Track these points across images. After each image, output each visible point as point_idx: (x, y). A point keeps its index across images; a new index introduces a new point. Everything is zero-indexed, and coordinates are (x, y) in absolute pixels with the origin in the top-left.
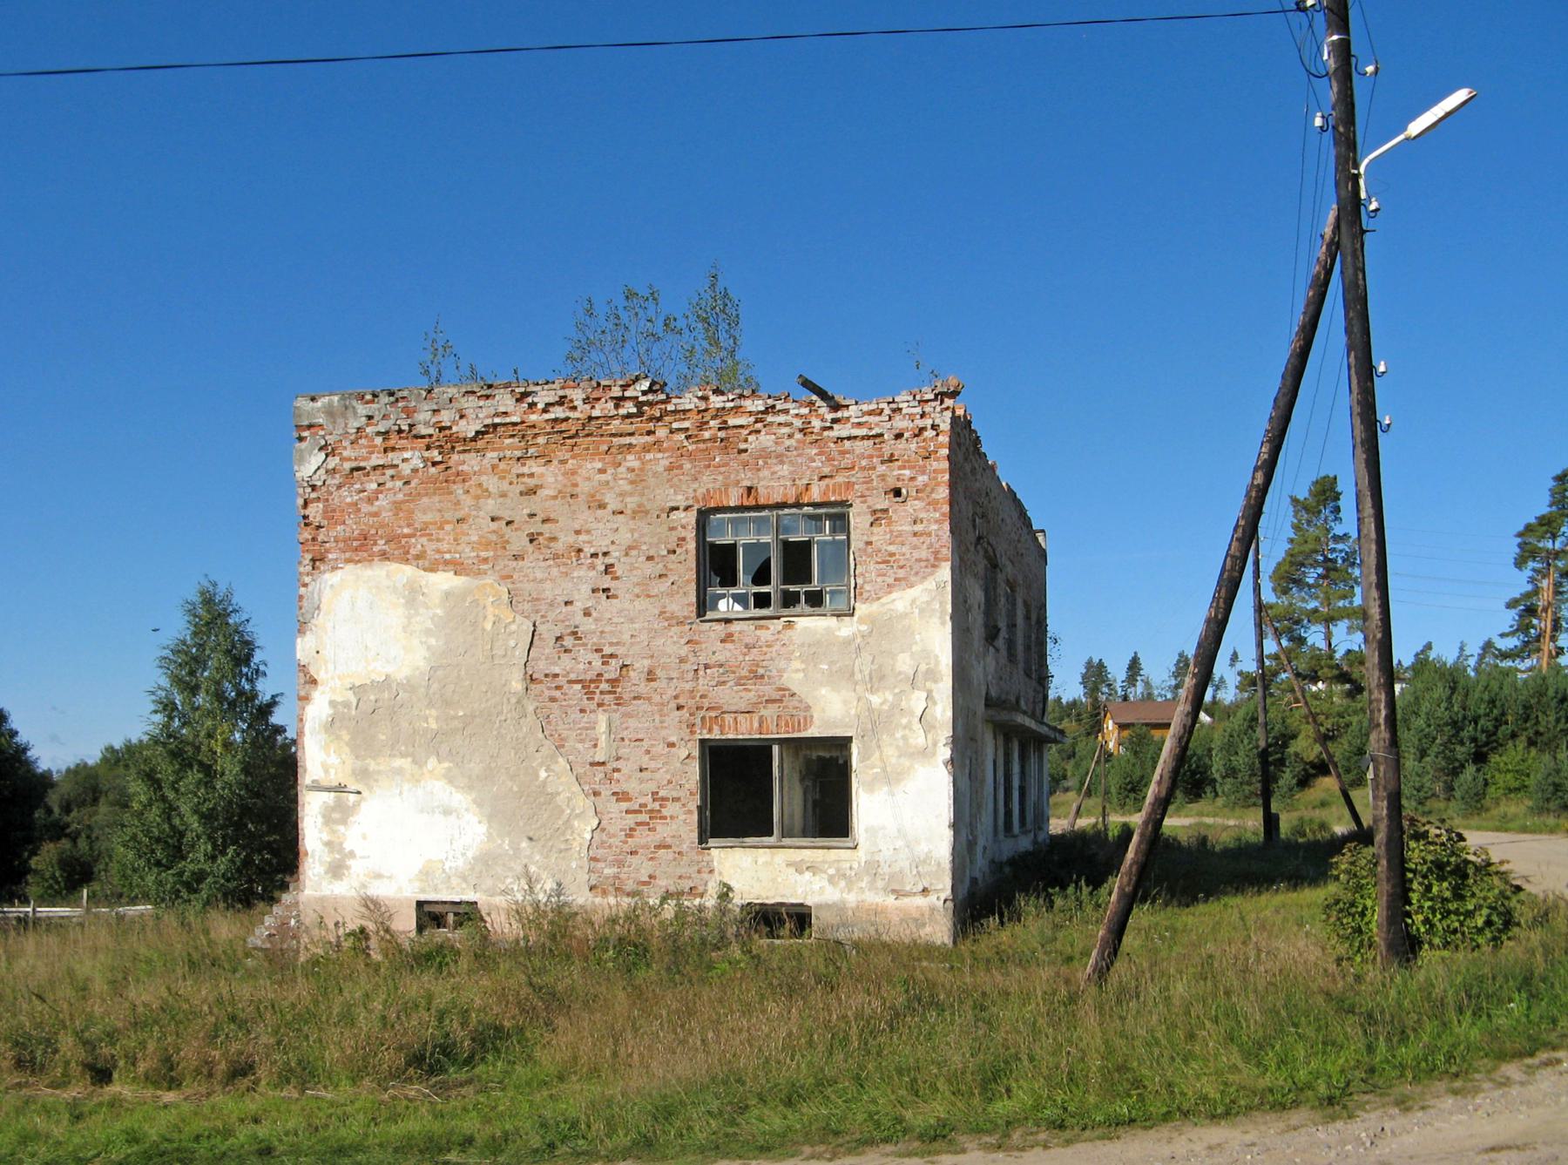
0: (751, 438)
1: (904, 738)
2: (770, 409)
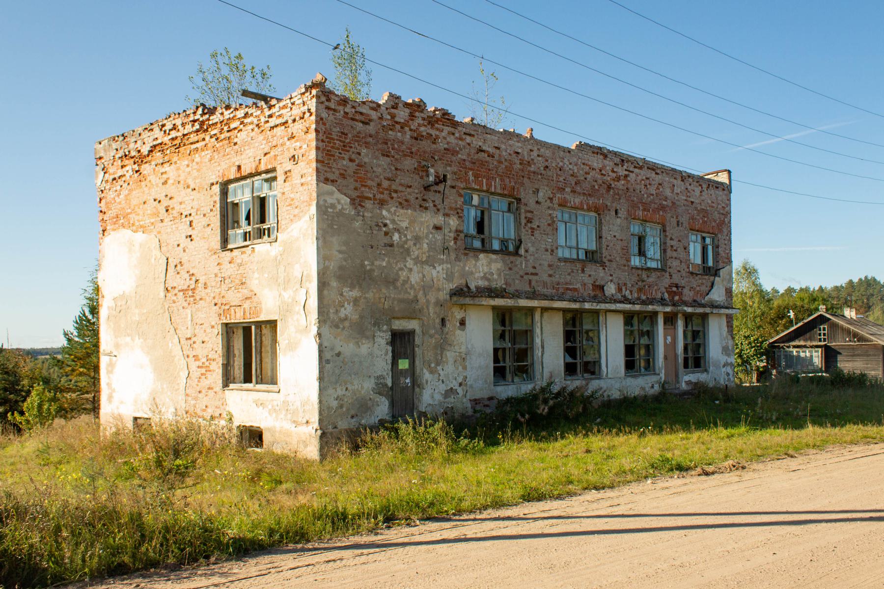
0: (239, 135)
1: (297, 320)
2: (246, 115)
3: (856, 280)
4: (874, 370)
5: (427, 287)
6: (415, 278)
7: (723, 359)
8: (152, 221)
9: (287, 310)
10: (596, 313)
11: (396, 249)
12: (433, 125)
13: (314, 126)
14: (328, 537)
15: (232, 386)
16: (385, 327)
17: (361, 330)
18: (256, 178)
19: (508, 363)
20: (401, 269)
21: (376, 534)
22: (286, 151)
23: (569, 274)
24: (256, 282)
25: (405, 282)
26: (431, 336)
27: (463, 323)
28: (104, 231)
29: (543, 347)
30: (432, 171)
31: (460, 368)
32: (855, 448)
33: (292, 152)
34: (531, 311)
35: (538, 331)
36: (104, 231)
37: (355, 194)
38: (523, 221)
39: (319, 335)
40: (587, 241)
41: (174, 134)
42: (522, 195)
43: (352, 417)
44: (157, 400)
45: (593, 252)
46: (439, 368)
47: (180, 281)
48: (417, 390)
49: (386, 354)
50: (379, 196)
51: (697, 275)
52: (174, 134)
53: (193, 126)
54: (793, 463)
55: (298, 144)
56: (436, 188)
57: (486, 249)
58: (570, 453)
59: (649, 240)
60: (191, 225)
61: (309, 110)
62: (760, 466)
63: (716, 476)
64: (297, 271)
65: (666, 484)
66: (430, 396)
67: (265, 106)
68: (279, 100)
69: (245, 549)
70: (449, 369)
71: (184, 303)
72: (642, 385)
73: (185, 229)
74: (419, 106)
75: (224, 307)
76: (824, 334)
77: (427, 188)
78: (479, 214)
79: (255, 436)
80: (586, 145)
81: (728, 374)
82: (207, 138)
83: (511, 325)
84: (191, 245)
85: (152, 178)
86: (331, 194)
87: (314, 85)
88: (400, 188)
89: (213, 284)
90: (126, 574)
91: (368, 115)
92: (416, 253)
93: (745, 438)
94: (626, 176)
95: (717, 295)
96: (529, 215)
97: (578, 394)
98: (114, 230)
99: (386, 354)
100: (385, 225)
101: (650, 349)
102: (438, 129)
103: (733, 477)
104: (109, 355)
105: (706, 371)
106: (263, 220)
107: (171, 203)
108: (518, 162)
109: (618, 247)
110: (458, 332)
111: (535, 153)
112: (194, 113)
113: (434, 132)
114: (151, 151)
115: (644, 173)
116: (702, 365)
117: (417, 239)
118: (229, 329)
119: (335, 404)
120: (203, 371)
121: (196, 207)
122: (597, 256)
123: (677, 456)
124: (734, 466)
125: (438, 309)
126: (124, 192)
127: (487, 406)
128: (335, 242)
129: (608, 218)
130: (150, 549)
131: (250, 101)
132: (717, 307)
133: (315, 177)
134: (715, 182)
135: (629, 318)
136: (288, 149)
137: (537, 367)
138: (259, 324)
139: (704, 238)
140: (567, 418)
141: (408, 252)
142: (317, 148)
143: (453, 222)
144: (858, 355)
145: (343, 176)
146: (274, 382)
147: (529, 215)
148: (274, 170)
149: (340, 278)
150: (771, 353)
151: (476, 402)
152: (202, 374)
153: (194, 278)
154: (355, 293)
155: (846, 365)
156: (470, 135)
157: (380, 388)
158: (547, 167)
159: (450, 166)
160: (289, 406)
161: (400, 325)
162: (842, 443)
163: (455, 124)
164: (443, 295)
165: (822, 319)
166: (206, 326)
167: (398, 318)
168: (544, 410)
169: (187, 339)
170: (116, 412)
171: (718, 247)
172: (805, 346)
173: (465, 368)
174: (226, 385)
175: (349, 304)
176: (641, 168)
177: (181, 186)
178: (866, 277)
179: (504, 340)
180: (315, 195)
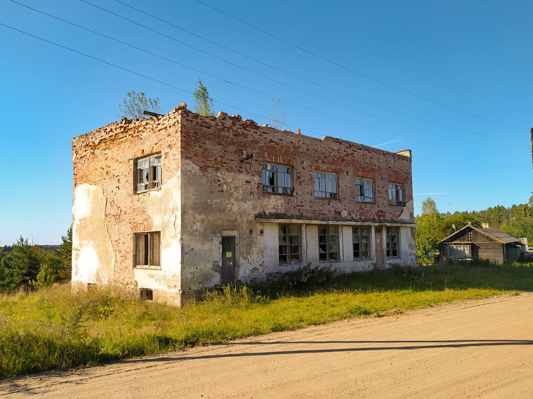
2: (147, 124)
3: (493, 207)
4: (498, 257)
5: (242, 213)
6: (235, 209)
7: (410, 251)
8: (100, 179)
9: (165, 226)
10: (337, 226)
11: (225, 193)
12: (245, 128)
13: (180, 129)
14: (157, 352)
15: (138, 267)
16: (219, 235)
17: (205, 237)
18: (152, 156)
19: (288, 254)
20: (228, 204)
21: (184, 351)
22: (165, 141)
23: (321, 206)
24: (150, 211)
25: (230, 211)
26: (244, 239)
27: (262, 232)
28: (76, 184)
29: (307, 245)
30: (244, 152)
31: (260, 256)
32: (470, 302)
33: (169, 143)
34: (300, 225)
35: (304, 236)
36: (76, 184)
37: (202, 165)
38: (295, 178)
39: (182, 239)
40: (331, 189)
41: (111, 134)
42: (295, 164)
43: (200, 283)
44: (100, 274)
45: (334, 194)
46: (248, 256)
47: (113, 211)
48: (236, 268)
49: (219, 249)
50: (215, 166)
51: (393, 206)
52: (111, 134)
53: (120, 129)
54: (430, 310)
55: (172, 139)
56: (247, 161)
57: (275, 192)
58: (287, 307)
59: (366, 187)
60: (119, 181)
61: (177, 121)
62: (412, 312)
63: (385, 317)
64: (171, 206)
65: (355, 322)
66: (244, 271)
67: (156, 119)
68: (163, 116)
69: (106, 360)
70: (254, 258)
71: (112, 221)
72: (363, 265)
73: (115, 183)
74: (237, 118)
75: (135, 225)
76: (471, 237)
77: (242, 161)
78: (271, 175)
79: (148, 293)
80: (330, 137)
81: (412, 260)
82: (127, 136)
83: (289, 233)
84: (119, 192)
85: (100, 157)
86: (189, 164)
87: (180, 108)
88: (227, 161)
89: (129, 212)
90: (37, 372)
91: (209, 123)
92: (236, 195)
93: (407, 296)
94: (352, 154)
95: (405, 216)
96: (298, 175)
97: (324, 271)
98: (81, 184)
99: (219, 249)
100: (219, 181)
101: (367, 245)
102: (248, 130)
103: (393, 318)
104: (76, 250)
105: (400, 257)
106: (155, 179)
107: (109, 170)
108: (292, 147)
109: (349, 191)
110: (259, 237)
111: (302, 142)
112: (121, 123)
113: (246, 132)
114: (99, 143)
115: (363, 152)
116: (397, 254)
117: (237, 188)
118: (137, 236)
119: (190, 276)
120: (123, 258)
121: (121, 172)
122: (337, 196)
123: (367, 306)
124: (396, 312)
125: (248, 225)
126: (86, 164)
127: (276, 277)
128: (191, 190)
129: (342, 176)
130: (53, 359)
131: (148, 117)
132: (404, 223)
133: (180, 156)
134: (402, 156)
135: (355, 229)
136: (167, 141)
137: (304, 256)
138: (152, 233)
139: (397, 186)
140: (317, 284)
141: (231, 194)
142: (182, 141)
143: (257, 179)
144: (489, 249)
145: (196, 155)
146: (159, 264)
147: (298, 175)
148: (160, 152)
149: (194, 209)
150: (441, 247)
151: (269, 275)
152: (123, 260)
153: (120, 209)
154: (202, 217)
155: (483, 255)
156: (265, 133)
157: (216, 268)
158: (308, 149)
159: (255, 149)
160: (165, 278)
161: (226, 233)
162: (463, 299)
163: (258, 128)
164: (251, 218)
165: (469, 229)
166: (125, 234)
167: (226, 230)
168: (304, 279)
169: (116, 241)
170: (79, 281)
171: (405, 191)
172: (460, 244)
173: (263, 256)
174: (135, 266)
175: (199, 222)
176: (361, 149)
177: (114, 160)
178: (498, 206)
179: (286, 241)
180: (180, 165)
